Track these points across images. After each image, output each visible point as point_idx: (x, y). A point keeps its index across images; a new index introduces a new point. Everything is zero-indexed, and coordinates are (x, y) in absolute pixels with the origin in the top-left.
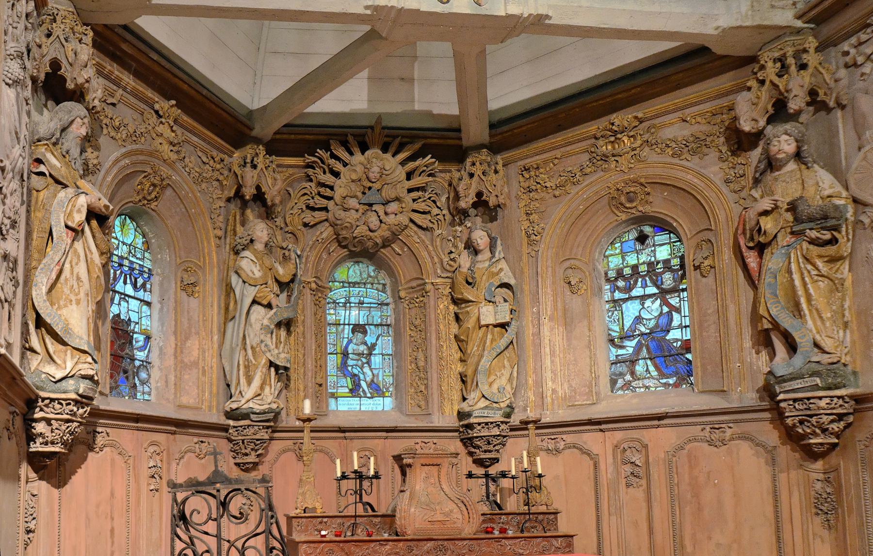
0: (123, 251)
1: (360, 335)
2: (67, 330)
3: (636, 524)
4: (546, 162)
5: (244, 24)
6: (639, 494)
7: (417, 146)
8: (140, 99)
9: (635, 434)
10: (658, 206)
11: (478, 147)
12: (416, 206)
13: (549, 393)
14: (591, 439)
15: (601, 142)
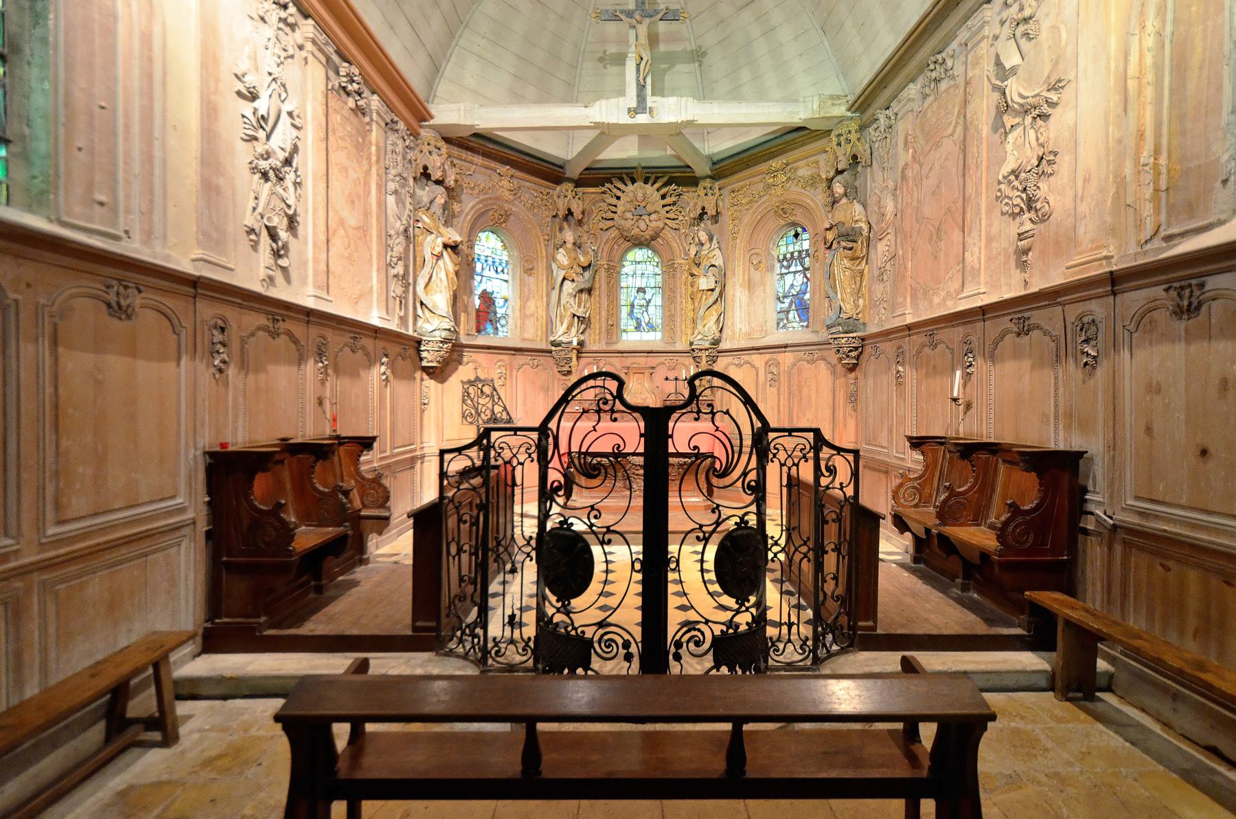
0: (488, 252)
2: (435, 306)
4: (742, 187)
6: (774, 390)
7: (665, 179)
9: (774, 356)
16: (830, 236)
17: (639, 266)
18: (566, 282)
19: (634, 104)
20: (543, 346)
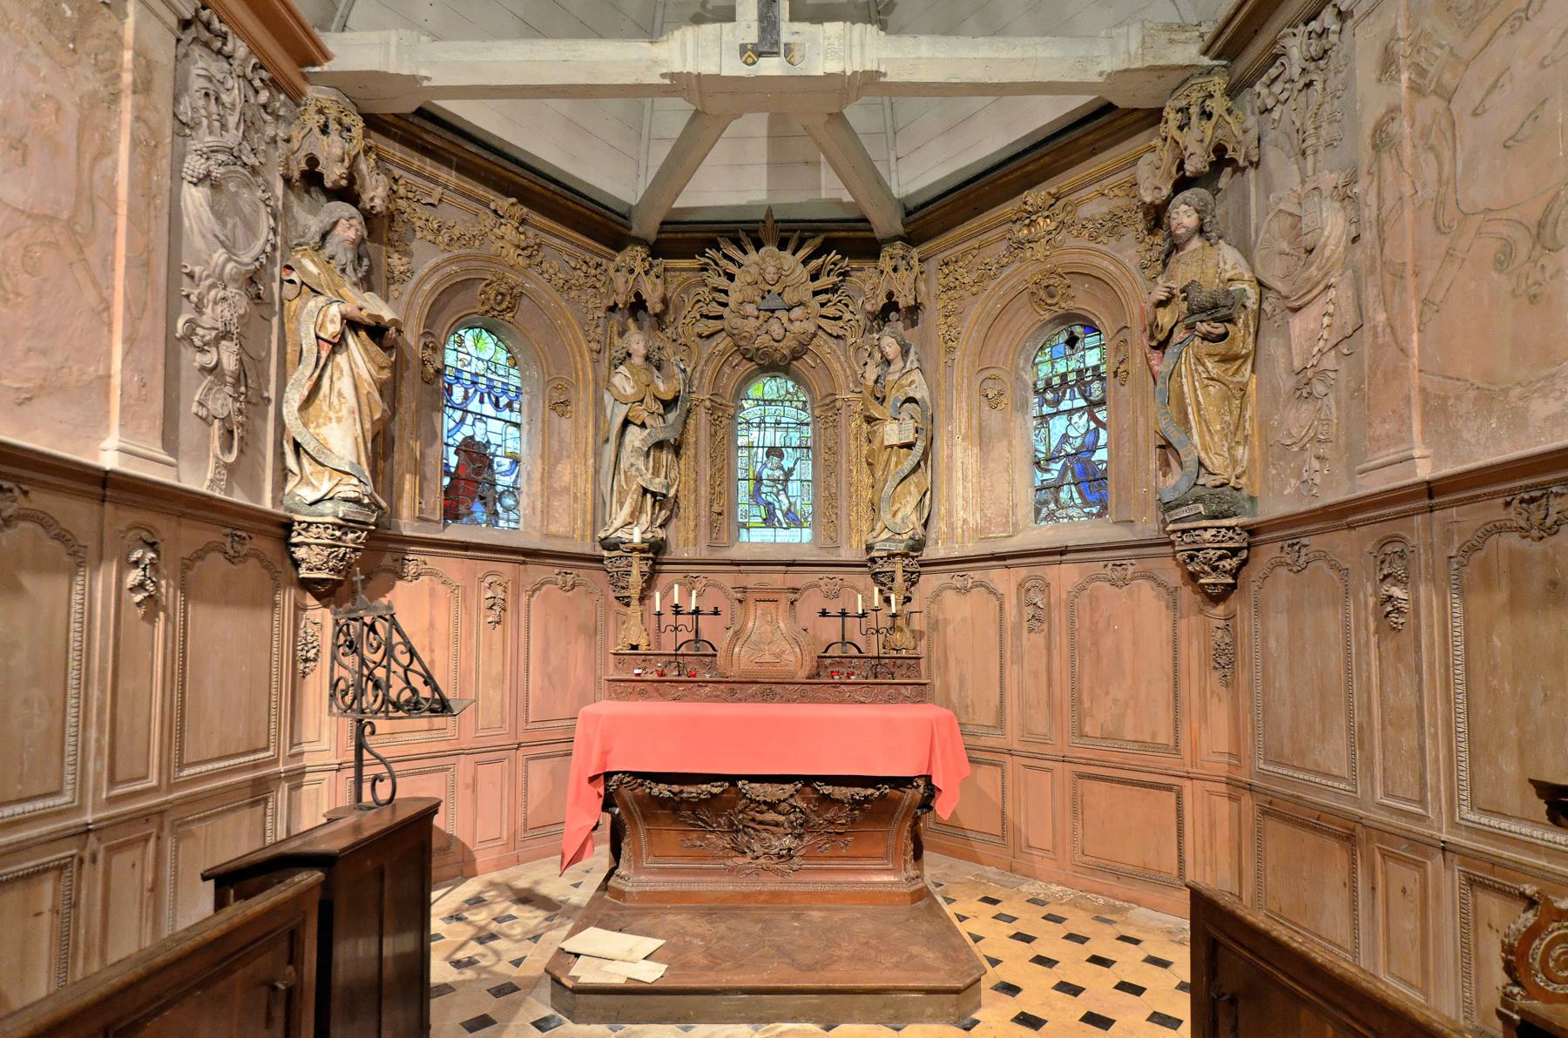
0: (479, 367)
1: (776, 459)
2: (324, 446)
3: (1036, 675)
4: (965, 253)
5: (616, 105)
6: (1040, 639)
7: (818, 241)
8: (469, 197)
9: (1038, 571)
10: (1082, 300)
11: (891, 240)
12: (824, 311)
13: (960, 523)
14: (998, 577)
15: (1017, 226)
16: (1166, 318)
17: (771, 409)
18: (632, 429)
19: (752, 37)
20: (587, 549)
